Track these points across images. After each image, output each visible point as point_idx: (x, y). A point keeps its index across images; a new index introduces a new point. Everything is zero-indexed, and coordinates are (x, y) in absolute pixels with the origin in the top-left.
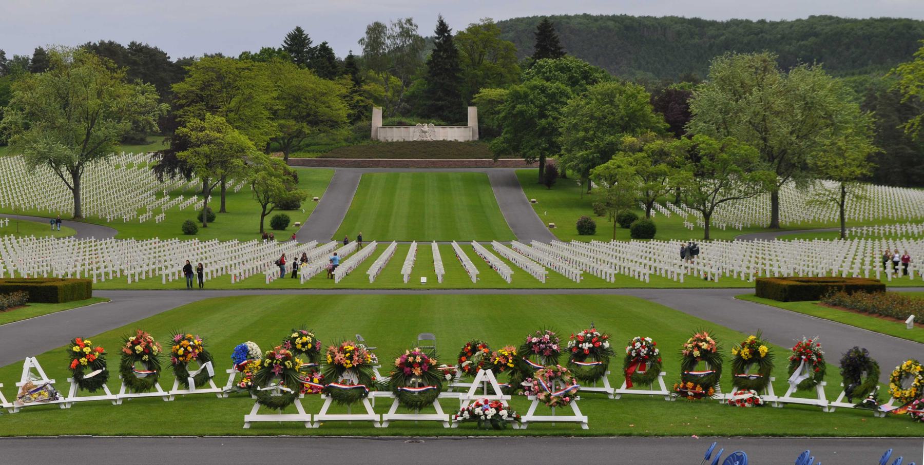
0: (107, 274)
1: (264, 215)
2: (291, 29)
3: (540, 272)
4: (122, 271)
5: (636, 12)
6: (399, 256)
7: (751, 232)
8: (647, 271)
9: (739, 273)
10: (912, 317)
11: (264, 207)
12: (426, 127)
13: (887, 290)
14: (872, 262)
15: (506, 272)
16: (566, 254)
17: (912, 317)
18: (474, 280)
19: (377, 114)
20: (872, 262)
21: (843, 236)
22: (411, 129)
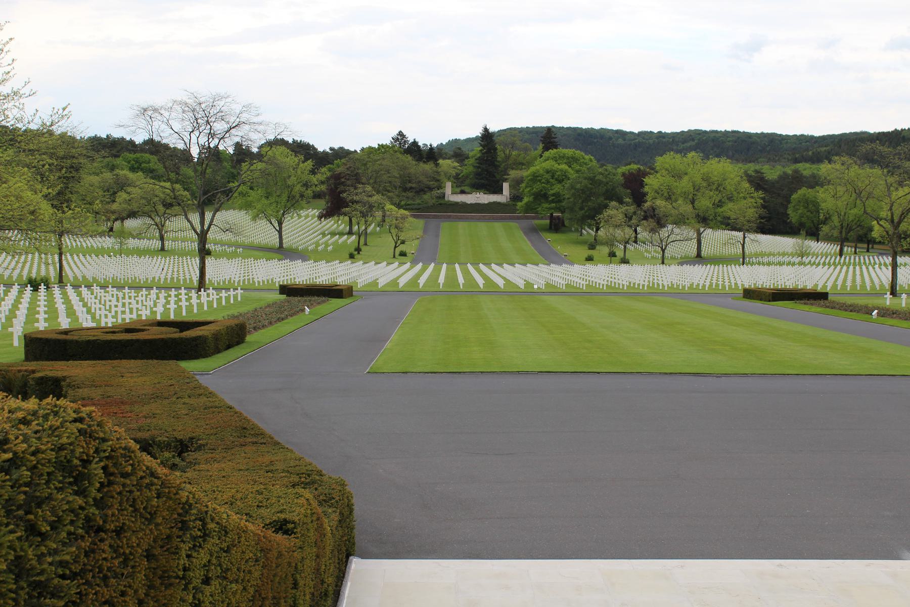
0: (249, 279)
1: (396, 247)
2: (394, 133)
3: (501, 283)
4: (272, 280)
5: (707, 127)
6: (437, 272)
7: (685, 261)
8: (584, 282)
9: (639, 285)
10: (876, 311)
11: (396, 243)
12: (478, 195)
13: (830, 298)
14: (178, 271)
15: (480, 282)
16: (537, 272)
17: (876, 311)
18: (482, 286)
19: (448, 188)
20: (178, 271)
21: (663, 263)
22: (469, 196)
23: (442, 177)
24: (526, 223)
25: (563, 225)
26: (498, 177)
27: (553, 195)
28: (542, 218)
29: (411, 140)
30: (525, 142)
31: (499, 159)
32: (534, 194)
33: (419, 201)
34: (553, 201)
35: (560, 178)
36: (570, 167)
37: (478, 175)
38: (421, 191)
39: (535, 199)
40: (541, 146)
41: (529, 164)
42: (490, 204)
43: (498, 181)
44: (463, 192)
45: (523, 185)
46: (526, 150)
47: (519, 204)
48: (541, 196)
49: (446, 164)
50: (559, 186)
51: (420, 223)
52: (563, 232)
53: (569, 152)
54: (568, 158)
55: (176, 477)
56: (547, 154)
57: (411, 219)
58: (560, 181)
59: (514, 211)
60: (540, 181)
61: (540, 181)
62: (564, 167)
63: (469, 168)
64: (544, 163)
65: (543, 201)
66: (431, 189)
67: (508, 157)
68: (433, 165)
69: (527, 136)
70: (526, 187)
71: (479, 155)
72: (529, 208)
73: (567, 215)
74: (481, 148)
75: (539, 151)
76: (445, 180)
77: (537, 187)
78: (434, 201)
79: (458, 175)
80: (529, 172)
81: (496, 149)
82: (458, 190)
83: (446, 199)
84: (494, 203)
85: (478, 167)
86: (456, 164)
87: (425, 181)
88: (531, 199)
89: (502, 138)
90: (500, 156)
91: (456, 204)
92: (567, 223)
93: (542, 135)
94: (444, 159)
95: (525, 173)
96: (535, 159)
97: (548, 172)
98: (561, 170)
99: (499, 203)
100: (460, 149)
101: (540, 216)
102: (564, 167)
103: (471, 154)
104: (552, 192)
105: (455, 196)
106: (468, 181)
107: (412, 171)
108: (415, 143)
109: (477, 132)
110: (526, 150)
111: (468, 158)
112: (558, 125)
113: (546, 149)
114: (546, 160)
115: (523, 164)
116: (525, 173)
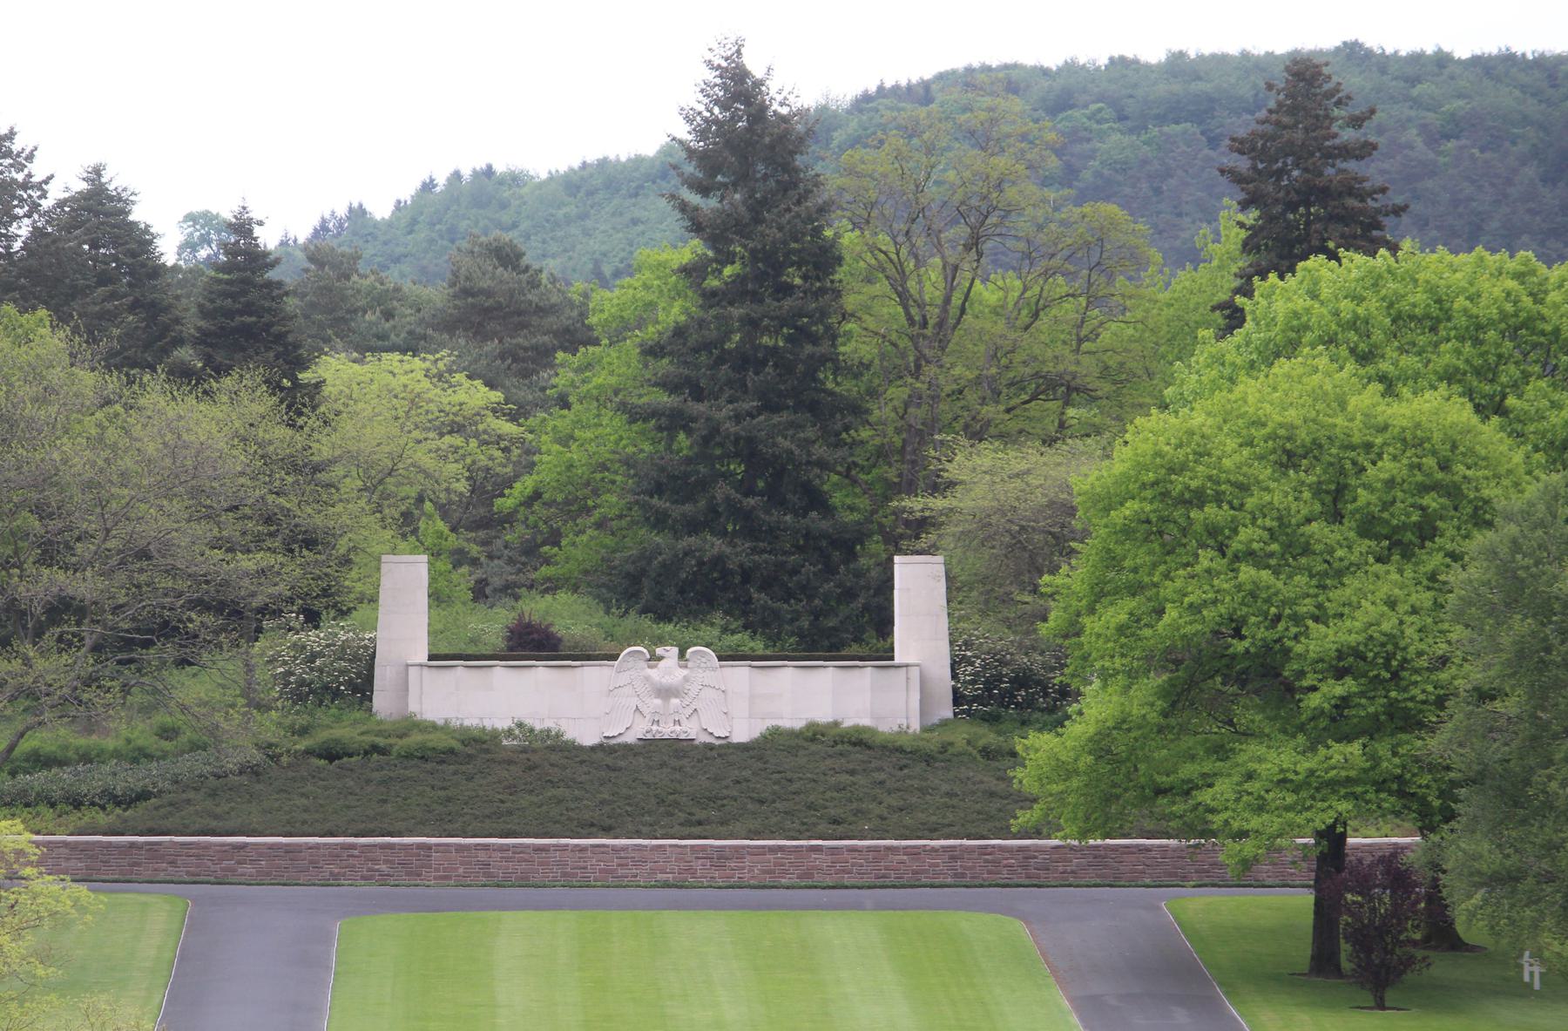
19: (402, 606)
22: (593, 675)
23: (348, 514)
24: (1104, 919)
25: (1444, 936)
26: (850, 506)
27: (1342, 664)
28: (1246, 876)
29: (62, 179)
30: (1103, 191)
31: (856, 346)
32: (1170, 658)
33: (141, 732)
34: (1338, 723)
35: (1403, 513)
36: (1492, 407)
37: (665, 488)
38: (146, 638)
39: (1178, 698)
40: (1232, 225)
41: (1124, 388)
42: (776, 748)
43: (847, 544)
44: (532, 644)
45: (1071, 579)
46: (1096, 262)
47: (1040, 747)
48: (1233, 677)
49: (377, 395)
50: (1392, 579)
51: (150, 921)
52: (1440, 997)
53: (1480, 276)
54: (1474, 331)
55: (1359, 503)
56: (1279, 297)
57: (52, 892)
58: (1399, 540)
59: (995, 809)
60: (1217, 538)
61: (1217, 538)
62: (1439, 409)
63: (587, 429)
64: (1259, 376)
65: (1249, 714)
66: (239, 618)
67: (933, 330)
68: (260, 404)
69: (1116, 143)
70: (1100, 594)
71: (674, 313)
72: (1129, 788)
73: (1469, 847)
74: (693, 249)
75: (1214, 277)
76: (377, 536)
77: (1193, 598)
78: (270, 726)
79: (486, 486)
80: (1122, 461)
81: (825, 259)
82: (493, 623)
83: (383, 702)
84: (814, 735)
85: (674, 422)
86: (476, 395)
87: (192, 545)
88: (1142, 698)
89: (878, 162)
90: (868, 320)
91: (474, 749)
92: (1470, 913)
93: (1243, 126)
94: (368, 346)
95: (1087, 472)
96: (1181, 342)
97: (1289, 456)
98: (1413, 441)
99: (858, 742)
100: (507, 257)
101: (1229, 852)
102: (1439, 409)
103: (607, 304)
104: (1323, 640)
105: (460, 674)
106: (581, 547)
107: (72, 455)
108: (100, 211)
109: (648, 114)
110: (1096, 262)
111: (576, 337)
112: (1398, 33)
113: (1278, 249)
114: (1273, 353)
115: (1070, 390)
116: (1087, 472)
